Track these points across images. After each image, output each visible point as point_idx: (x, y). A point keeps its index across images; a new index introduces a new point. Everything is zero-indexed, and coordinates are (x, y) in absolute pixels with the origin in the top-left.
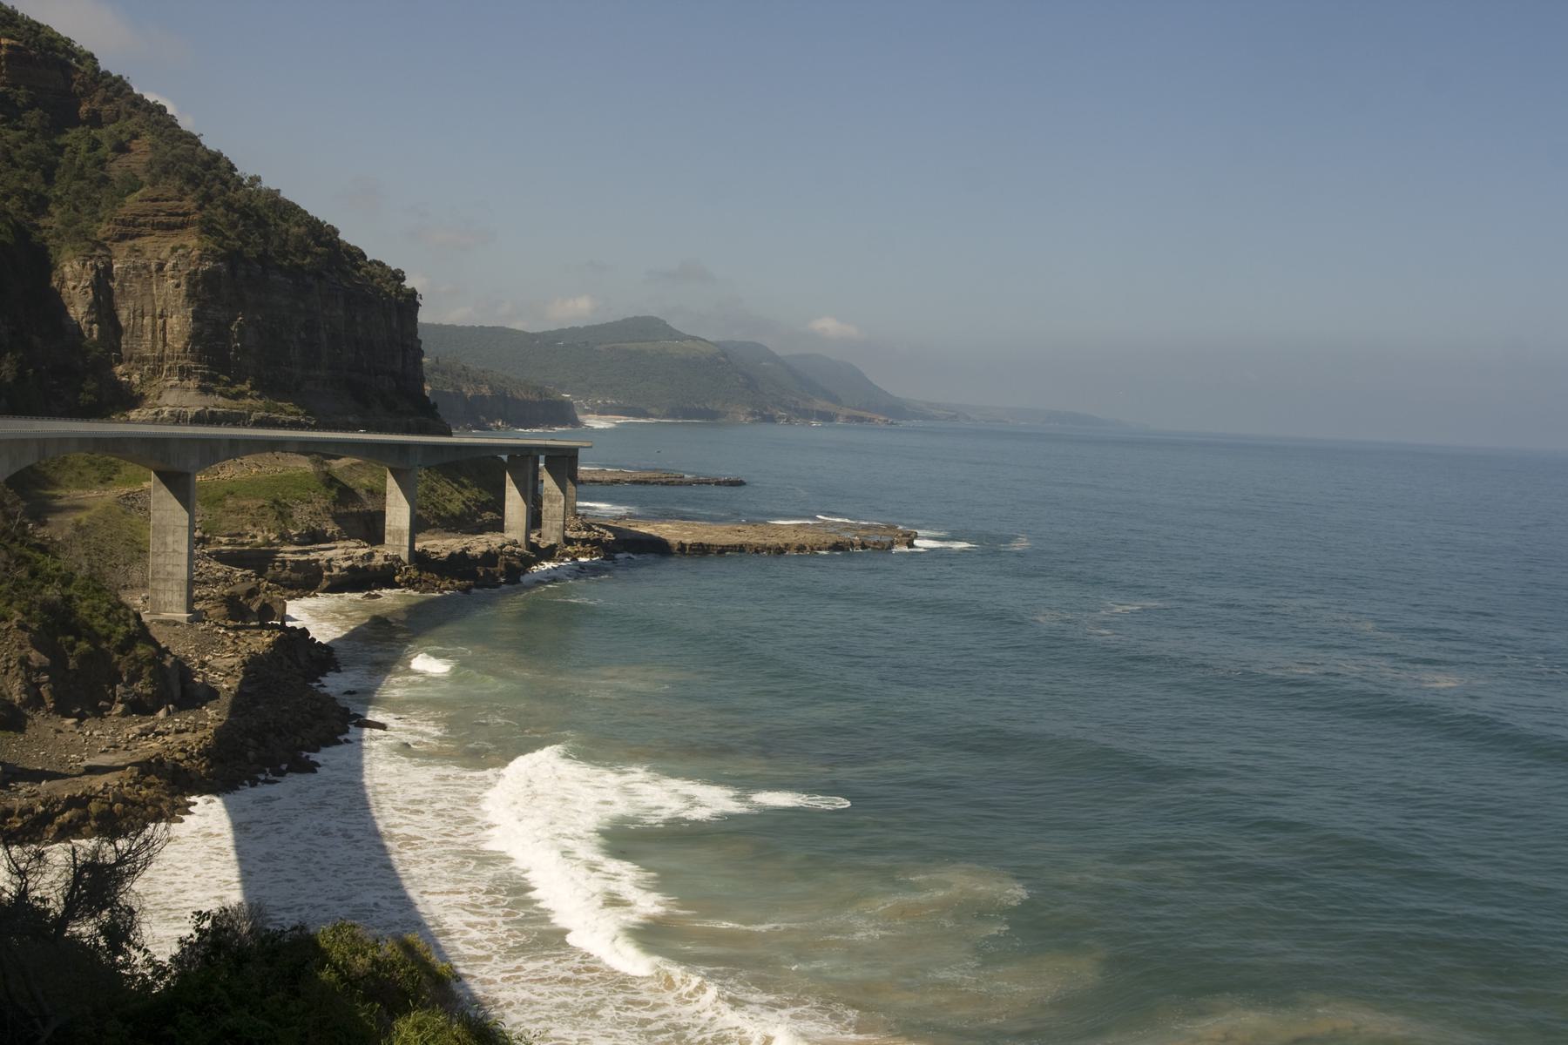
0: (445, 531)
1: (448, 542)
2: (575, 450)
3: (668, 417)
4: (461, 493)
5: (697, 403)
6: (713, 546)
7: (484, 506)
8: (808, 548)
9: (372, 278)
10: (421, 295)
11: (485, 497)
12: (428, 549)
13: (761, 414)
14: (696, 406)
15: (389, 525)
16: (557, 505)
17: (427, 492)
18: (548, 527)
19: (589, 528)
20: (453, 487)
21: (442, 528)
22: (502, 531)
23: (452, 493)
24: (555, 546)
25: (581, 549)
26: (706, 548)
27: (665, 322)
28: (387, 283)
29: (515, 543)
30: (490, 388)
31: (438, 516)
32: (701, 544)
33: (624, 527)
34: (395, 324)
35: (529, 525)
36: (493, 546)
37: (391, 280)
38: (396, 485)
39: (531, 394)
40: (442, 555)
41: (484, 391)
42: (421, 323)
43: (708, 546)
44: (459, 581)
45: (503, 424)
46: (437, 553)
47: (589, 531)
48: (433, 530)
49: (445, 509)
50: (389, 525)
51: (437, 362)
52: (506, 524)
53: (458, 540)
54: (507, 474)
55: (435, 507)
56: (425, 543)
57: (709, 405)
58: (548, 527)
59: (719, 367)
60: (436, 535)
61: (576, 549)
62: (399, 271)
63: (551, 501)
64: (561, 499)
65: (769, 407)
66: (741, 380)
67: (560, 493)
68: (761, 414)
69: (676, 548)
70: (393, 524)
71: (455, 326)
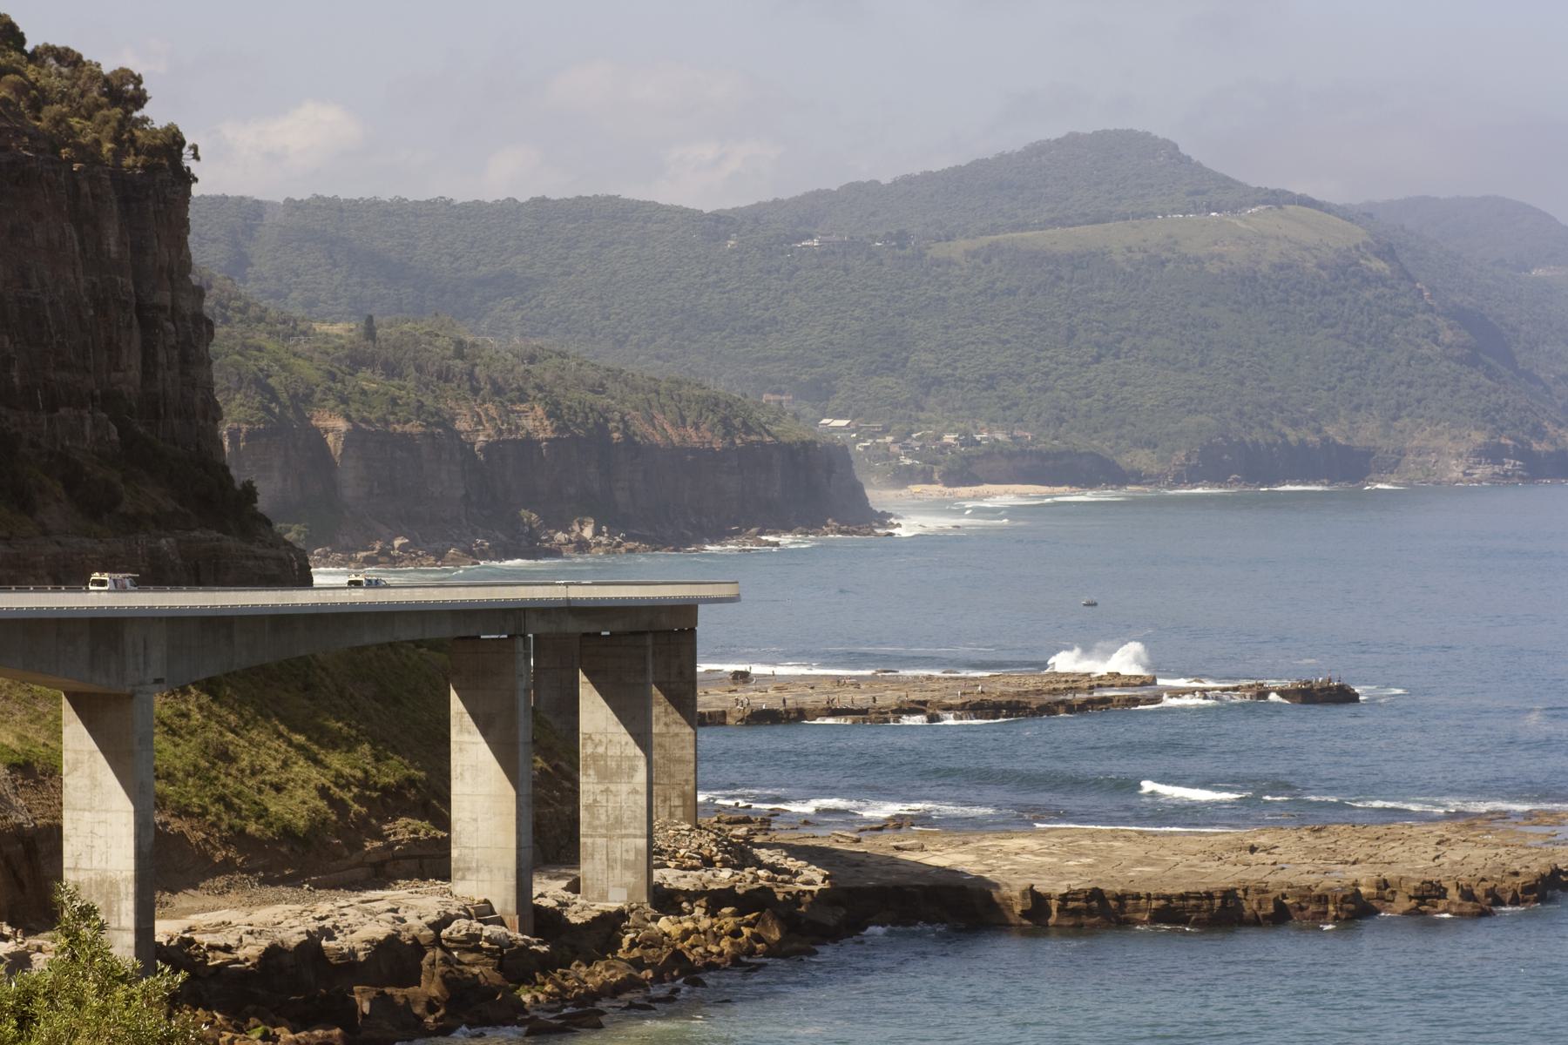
0: (263, 882)
1: (263, 915)
2: (686, 611)
3: (1193, 478)
4: (317, 762)
5: (1295, 424)
6: (1137, 897)
7: (392, 801)
8: (1453, 894)
9: (36, 106)
10: (195, 148)
11: (391, 773)
12: (197, 938)
13: (1524, 454)
14: (1292, 436)
15: (75, 869)
16: (624, 788)
17: (204, 764)
18: (600, 856)
19: (741, 856)
20: (290, 743)
21: (251, 872)
22: (446, 876)
23: (285, 765)
24: (621, 915)
25: (705, 923)
26: (1113, 903)
27: (1176, 147)
28: (89, 117)
29: (484, 912)
30: (549, 415)
31: (239, 838)
32: (1096, 894)
33: (880, 852)
34: (112, 245)
35: (529, 854)
36: (411, 920)
37: (99, 107)
38: (90, 744)
39: (696, 426)
40: (241, 954)
41: (528, 423)
42: (249, 213)
43: (1121, 898)
44: (294, 1032)
45: (597, 532)
46: (227, 949)
47: (741, 868)
48: (220, 881)
49: (262, 814)
50: (75, 869)
51: (370, 332)
52: (455, 853)
53: (298, 908)
54: (454, 695)
55: (229, 806)
56: (193, 920)
57: (1335, 432)
58: (600, 856)
59: (1368, 294)
60: (232, 896)
61: (689, 925)
62: (126, 75)
63: (605, 775)
64: (633, 769)
65: (1550, 428)
66: (1447, 336)
67: (639, 752)
68: (1524, 454)
69: (1018, 909)
70: (84, 864)
71: (449, 203)
